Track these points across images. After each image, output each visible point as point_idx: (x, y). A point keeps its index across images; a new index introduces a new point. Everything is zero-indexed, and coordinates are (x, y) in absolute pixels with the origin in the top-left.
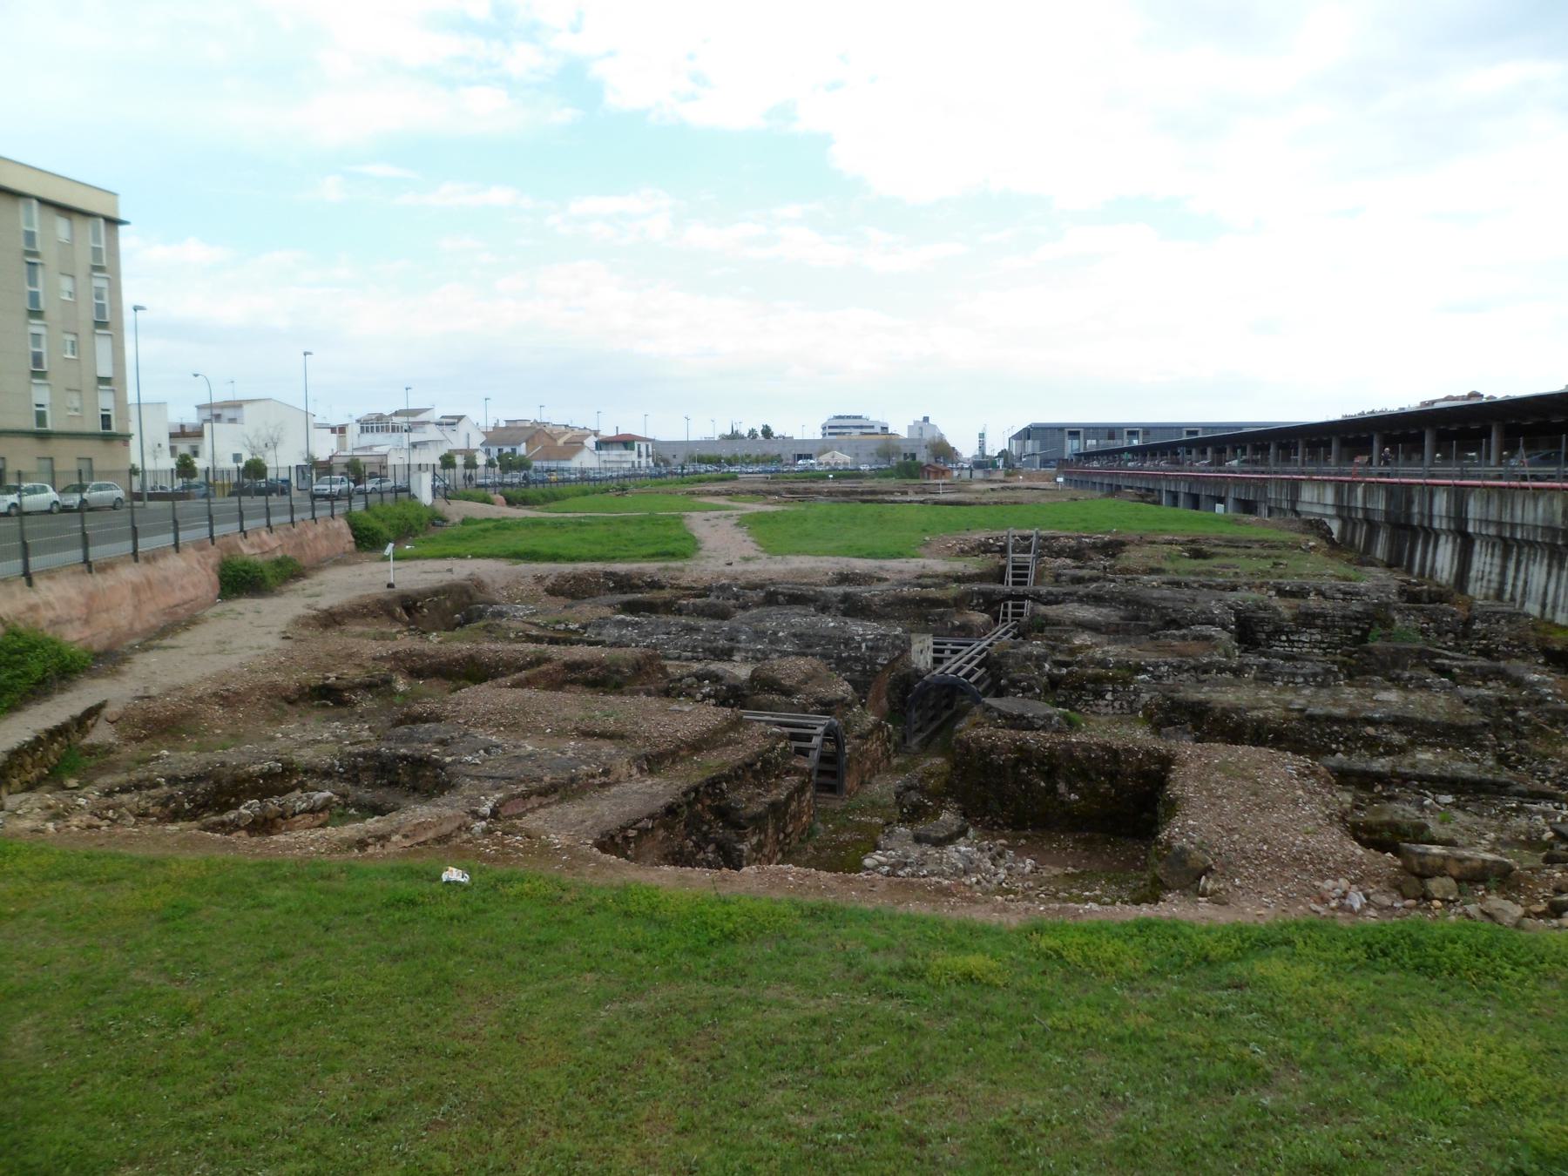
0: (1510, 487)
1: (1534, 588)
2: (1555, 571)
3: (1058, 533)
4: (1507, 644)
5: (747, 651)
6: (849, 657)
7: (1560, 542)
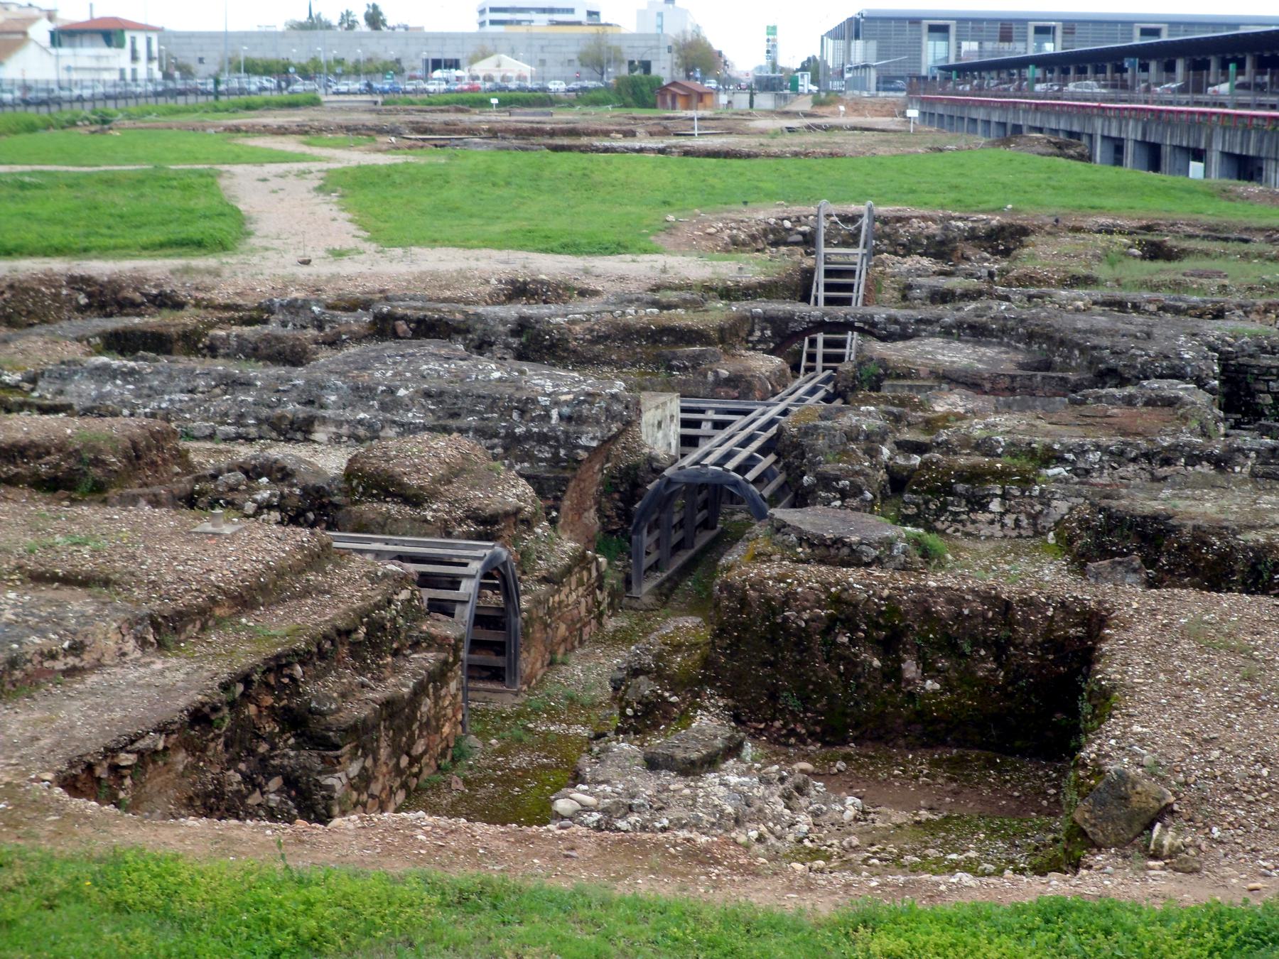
5: (339, 424)
6: (529, 436)
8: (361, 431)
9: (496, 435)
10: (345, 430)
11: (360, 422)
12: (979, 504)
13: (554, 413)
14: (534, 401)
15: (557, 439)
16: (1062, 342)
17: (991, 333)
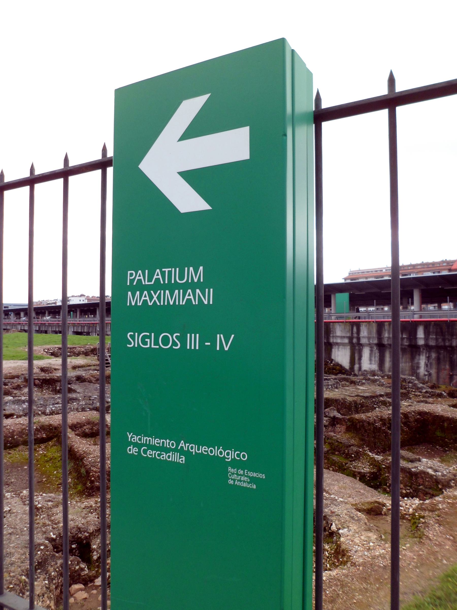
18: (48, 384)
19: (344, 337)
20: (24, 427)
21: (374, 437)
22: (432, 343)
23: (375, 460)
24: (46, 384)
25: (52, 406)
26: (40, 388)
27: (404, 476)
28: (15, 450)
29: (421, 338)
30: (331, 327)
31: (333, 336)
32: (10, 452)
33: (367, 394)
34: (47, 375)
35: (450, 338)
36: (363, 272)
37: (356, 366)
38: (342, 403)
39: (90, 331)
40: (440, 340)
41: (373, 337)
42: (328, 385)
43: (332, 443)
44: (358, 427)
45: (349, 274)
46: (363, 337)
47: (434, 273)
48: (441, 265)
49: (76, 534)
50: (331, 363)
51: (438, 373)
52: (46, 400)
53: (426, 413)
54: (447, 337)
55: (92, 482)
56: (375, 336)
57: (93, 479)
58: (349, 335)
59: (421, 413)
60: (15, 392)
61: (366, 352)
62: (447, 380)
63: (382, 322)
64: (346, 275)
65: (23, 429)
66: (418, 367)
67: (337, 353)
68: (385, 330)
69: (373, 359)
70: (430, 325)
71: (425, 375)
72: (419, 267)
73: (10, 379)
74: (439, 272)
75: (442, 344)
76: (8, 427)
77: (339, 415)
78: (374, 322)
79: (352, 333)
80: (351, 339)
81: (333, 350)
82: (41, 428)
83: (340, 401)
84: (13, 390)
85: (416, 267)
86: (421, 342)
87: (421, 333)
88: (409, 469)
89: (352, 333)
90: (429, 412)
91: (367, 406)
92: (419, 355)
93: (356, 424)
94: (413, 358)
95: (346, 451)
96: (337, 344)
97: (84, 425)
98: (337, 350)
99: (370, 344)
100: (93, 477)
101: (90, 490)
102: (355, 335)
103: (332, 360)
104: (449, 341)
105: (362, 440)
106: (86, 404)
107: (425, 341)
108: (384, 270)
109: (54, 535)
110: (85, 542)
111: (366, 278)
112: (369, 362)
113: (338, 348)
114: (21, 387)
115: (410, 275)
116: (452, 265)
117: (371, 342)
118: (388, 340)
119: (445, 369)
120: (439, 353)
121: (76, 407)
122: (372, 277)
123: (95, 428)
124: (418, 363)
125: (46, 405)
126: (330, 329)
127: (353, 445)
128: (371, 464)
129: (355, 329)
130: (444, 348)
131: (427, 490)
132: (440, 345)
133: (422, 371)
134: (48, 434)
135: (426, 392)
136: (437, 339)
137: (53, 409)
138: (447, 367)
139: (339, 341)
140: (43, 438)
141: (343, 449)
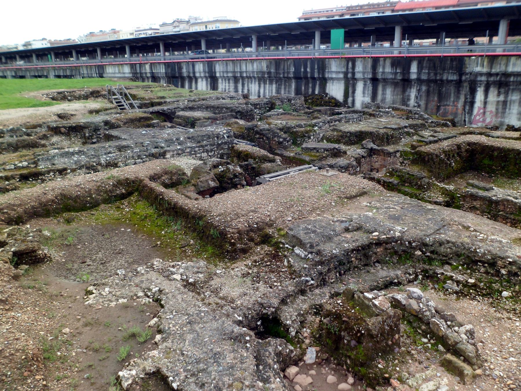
0: (237, 60)
1: (253, 91)
2: (262, 85)
3: (75, 90)
4: (299, 106)
5: (173, 151)
6: (222, 143)
7: (266, 76)
8: (180, 152)
9: (214, 145)
10: (175, 152)
11: (179, 149)
12: (309, 138)
13: (225, 136)
14: (219, 134)
15: (229, 142)
16: (218, 107)
17: (195, 108)
18: (75, 132)
19: (339, 72)
20: (99, 184)
21: (439, 168)
22: (424, 77)
23: (447, 190)
24: (73, 132)
25: (105, 156)
26: (68, 136)
27: (482, 204)
28: (97, 210)
29: (414, 73)
30: (327, 63)
31: (328, 72)
32: (92, 213)
33: (394, 126)
34: (65, 122)
35: (441, 72)
36: (316, 12)
37: (350, 100)
38: (377, 136)
39: (74, 74)
40: (432, 74)
41: (368, 72)
42: (354, 118)
43: (403, 176)
44: (426, 159)
45: (303, 13)
46: (358, 72)
47: (379, 13)
48: (385, 6)
49: (260, 310)
50: (326, 96)
51: (427, 105)
52: (96, 150)
53: (475, 144)
54: (438, 71)
55: (233, 245)
56: (369, 71)
57: (233, 241)
58: (344, 70)
59: (469, 144)
60: (43, 142)
61: (360, 86)
62: (434, 111)
63: (377, 57)
64: (300, 15)
65: (99, 187)
66: (409, 100)
67: (331, 87)
68: (380, 65)
69: (366, 92)
70: (424, 60)
71: (415, 106)
72: (366, 7)
73: (33, 128)
74: (383, 13)
75: (434, 78)
76: (82, 186)
77: (375, 147)
78: (369, 57)
79: (347, 68)
80: (346, 74)
81: (328, 84)
82: (117, 183)
83: (375, 134)
84: (40, 141)
85: (363, 8)
86: (414, 76)
87: (414, 68)
88: (490, 197)
89: (347, 68)
90: (477, 143)
91: (396, 137)
92: (411, 88)
93: (425, 157)
94: (404, 91)
95: (419, 182)
96: (332, 79)
97: (162, 176)
98: (331, 84)
99: (364, 79)
100: (233, 239)
101: (232, 252)
102: (350, 70)
103: (327, 94)
104: (440, 75)
105: (431, 171)
106: (140, 151)
107: (418, 76)
108: (334, 10)
109: (239, 316)
110: (271, 317)
111: (319, 18)
112: (362, 95)
113: (333, 83)
114: (47, 137)
115: (358, 14)
116: (395, 6)
117: (366, 76)
118: (382, 75)
119: (433, 101)
120: (429, 86)
121: (131, 155)
122: (323, 17)
123: (174, 178)
124: (409, 96)
125: (99, 156)
126: (326, 65)
127: (425, 177)
128: (443, 194)
129: (350, 65)
130: (435, 81)
131: (507, 215)
132: (431, 79)
133: (412, 102)
134: (127, 188)
135: (432, 122)
136: (429, 74)
137: (108, 159)
138: (436, 99)
139: (334, 76)
140: (123, 194)
141: (415, 181)
